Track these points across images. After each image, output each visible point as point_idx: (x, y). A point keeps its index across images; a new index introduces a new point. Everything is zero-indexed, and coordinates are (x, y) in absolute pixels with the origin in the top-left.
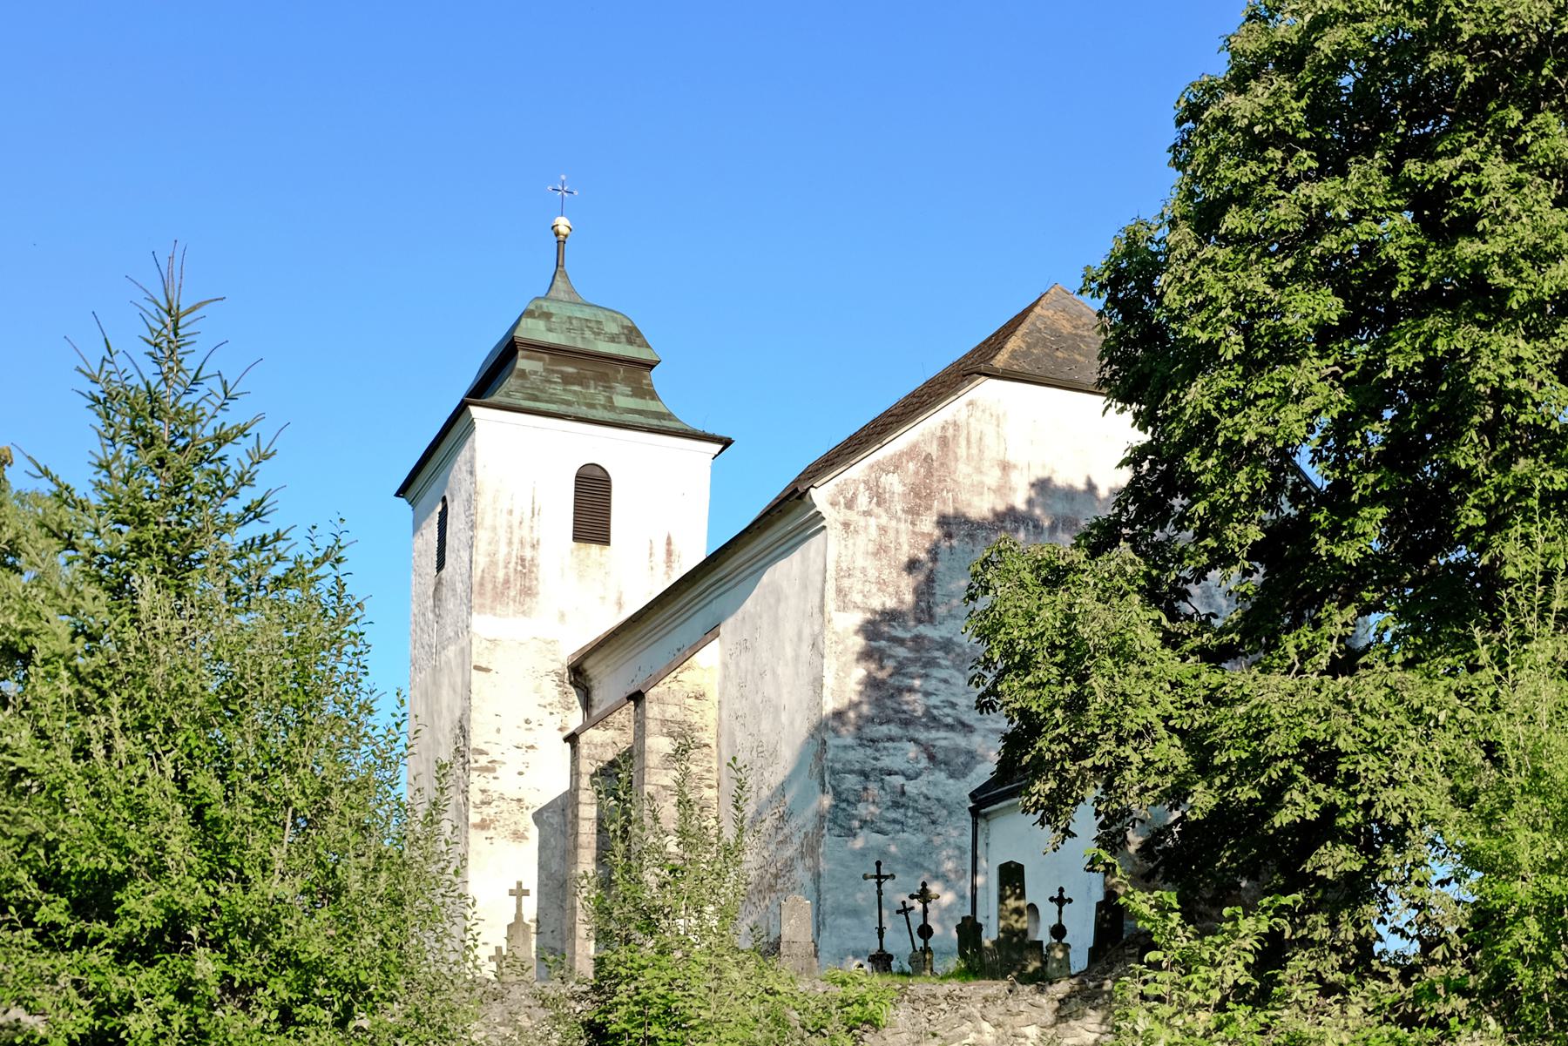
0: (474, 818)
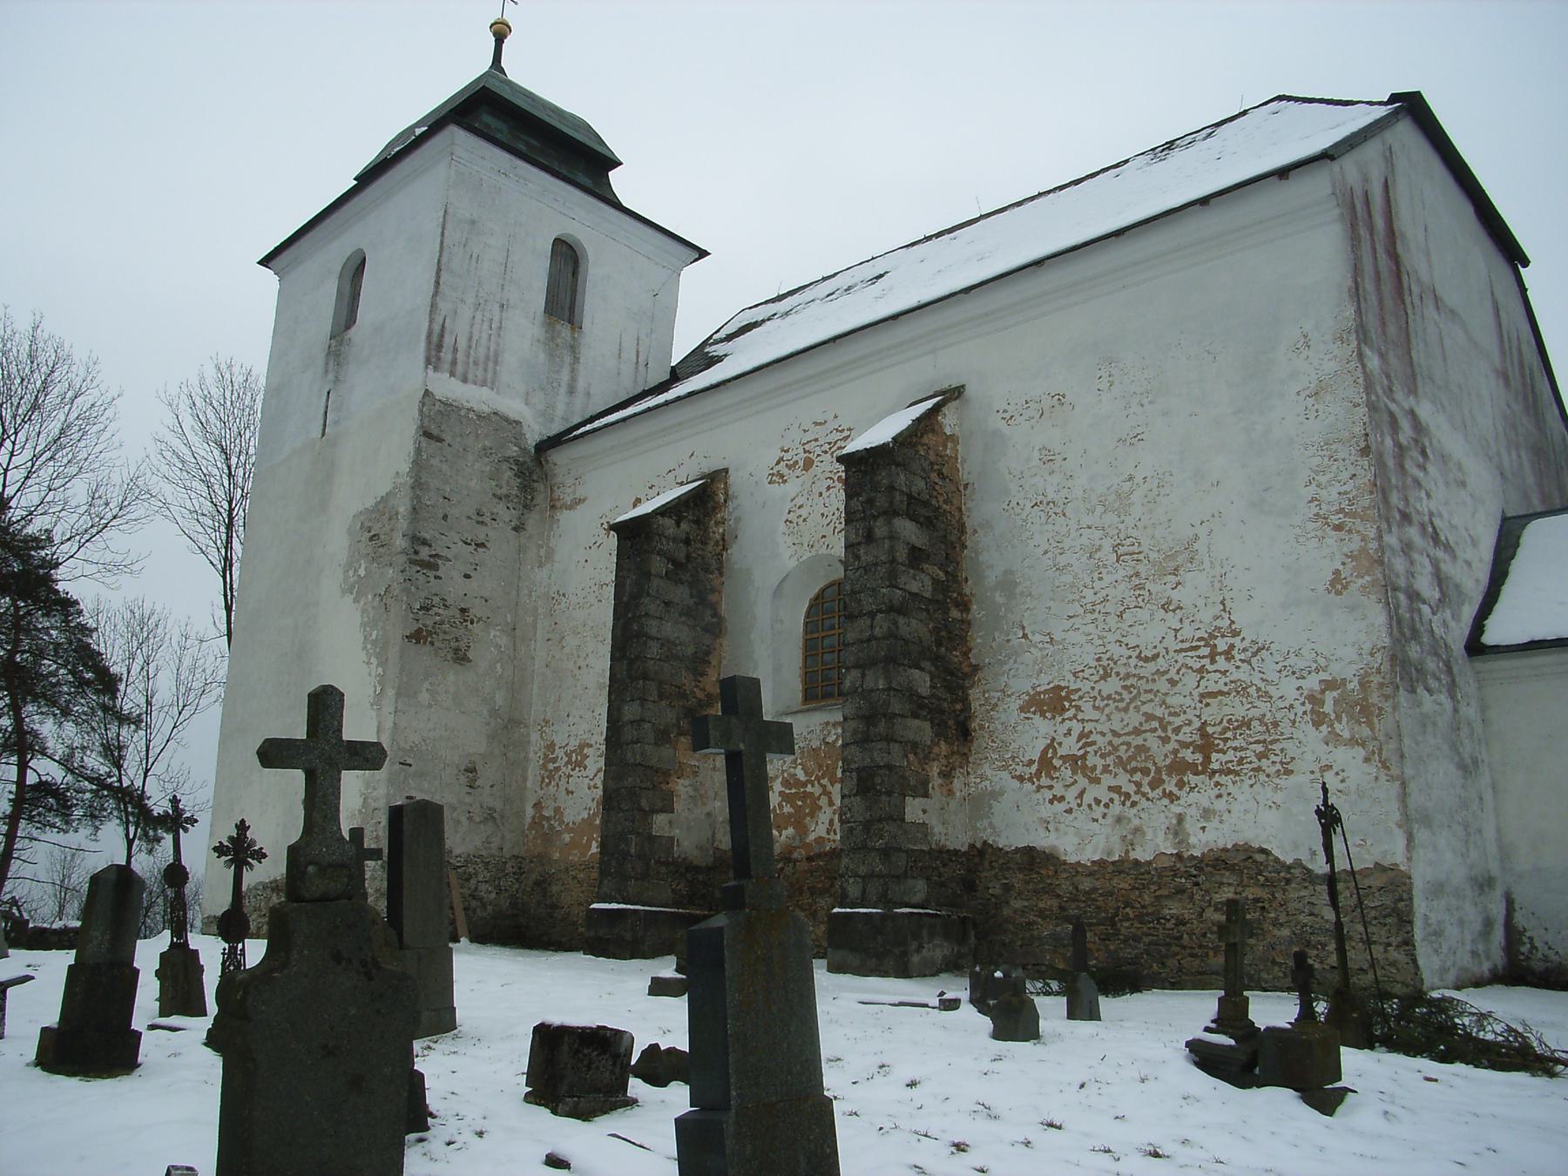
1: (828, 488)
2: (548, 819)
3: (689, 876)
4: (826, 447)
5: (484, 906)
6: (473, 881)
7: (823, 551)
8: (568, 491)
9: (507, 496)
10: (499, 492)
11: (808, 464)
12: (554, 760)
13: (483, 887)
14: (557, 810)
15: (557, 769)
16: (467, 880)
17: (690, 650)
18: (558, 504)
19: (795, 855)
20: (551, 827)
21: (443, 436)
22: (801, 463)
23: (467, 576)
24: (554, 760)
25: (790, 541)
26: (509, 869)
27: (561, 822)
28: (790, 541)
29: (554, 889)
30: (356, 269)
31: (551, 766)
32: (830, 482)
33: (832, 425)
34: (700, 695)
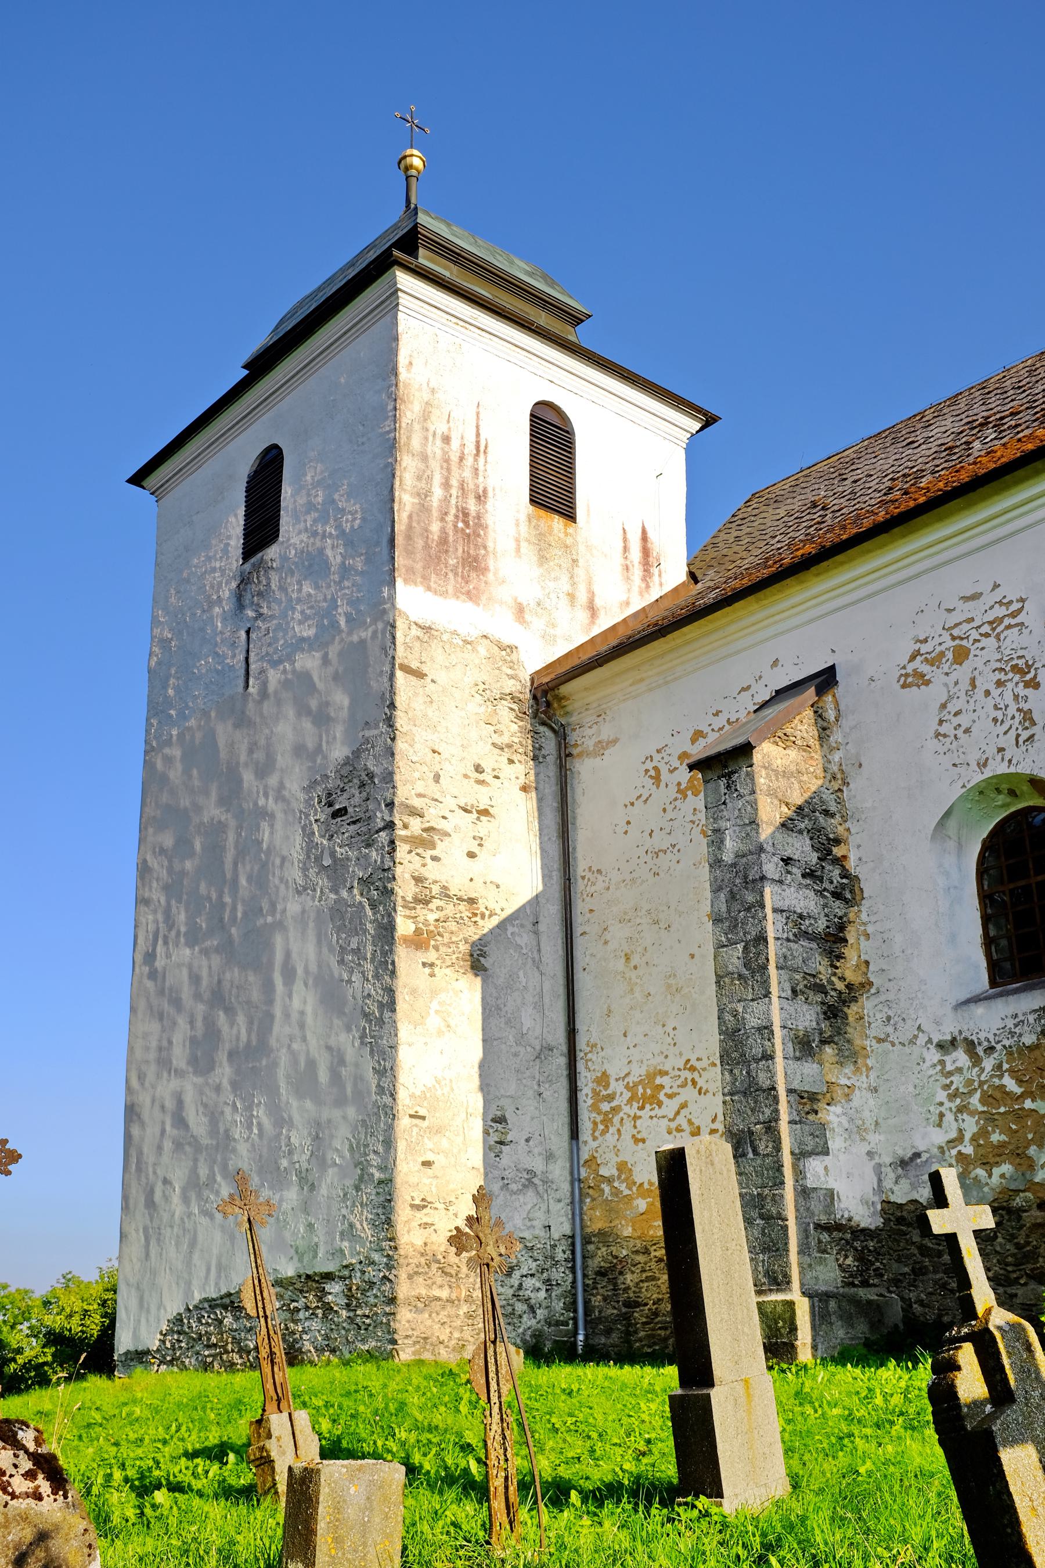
0: (404, 926)
1: (999, 683)
2: (609, 1180)
3: (857, 1244)
4: (986, 629)
5: (532, 1309)
6: (517, 1274)
7: (1003, 769)
8: (588, 732)
9: (509, 746)
10: (498, 740)
11: (961, 655)
12: (611, 1098)
13: (529, 1283)
14: (622, 1167)
15: (615, 1110)
16: (509, 1274)
17: (821, 925)
18: (575, 752)
19: (1018, 1201)
20: (616, 1192)
21: (425, 669)
22: (950, 655)
23: (471, 855)
24: (611, 1098)
25: (947, 761)
26: (560, 1256)
27: (631, 1184)
28: (947, 761)
29: (630, 1279)
30: (269, 469)
31: (605, 1107)
32: (998, 676)
33: (989, 599)
34: (840, 986)
